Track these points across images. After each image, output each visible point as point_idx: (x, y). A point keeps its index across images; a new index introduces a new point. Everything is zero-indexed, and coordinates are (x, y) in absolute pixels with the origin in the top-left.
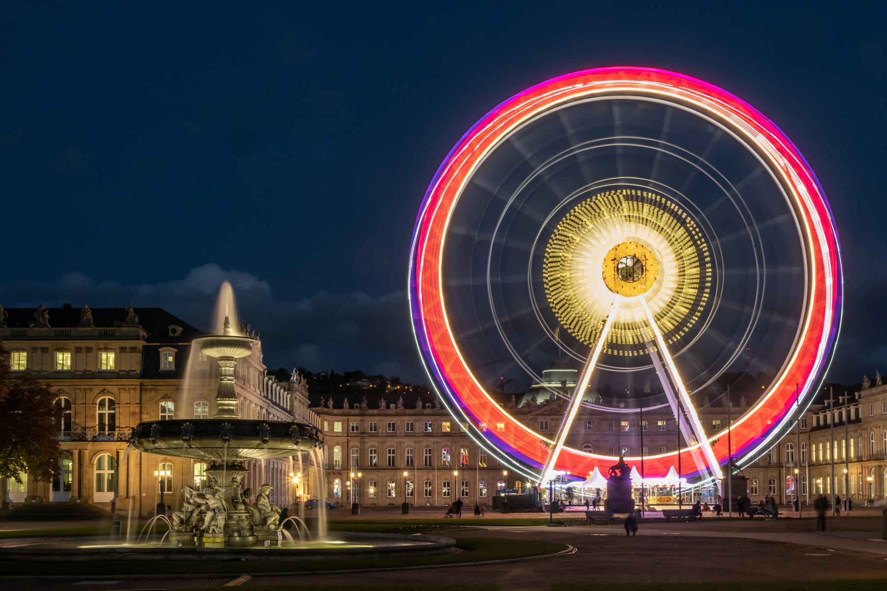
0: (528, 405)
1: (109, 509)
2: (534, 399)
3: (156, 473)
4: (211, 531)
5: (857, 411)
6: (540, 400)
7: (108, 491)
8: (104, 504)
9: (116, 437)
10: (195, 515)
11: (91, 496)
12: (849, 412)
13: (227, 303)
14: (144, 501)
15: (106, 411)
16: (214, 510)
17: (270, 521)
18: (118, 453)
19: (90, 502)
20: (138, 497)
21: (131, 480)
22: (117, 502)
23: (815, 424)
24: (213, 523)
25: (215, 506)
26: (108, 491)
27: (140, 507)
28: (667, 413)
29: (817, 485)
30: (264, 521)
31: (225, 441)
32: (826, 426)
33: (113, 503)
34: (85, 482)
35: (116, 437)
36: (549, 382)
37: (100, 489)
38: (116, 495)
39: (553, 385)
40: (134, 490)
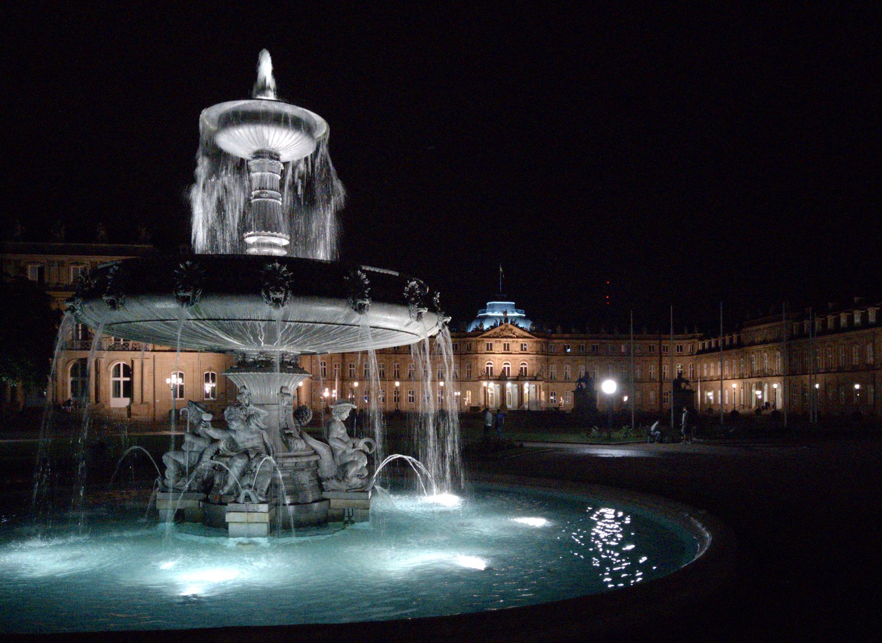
0: (477, 329)
1: (125, 413)
2: (481, 325)
3: (168, 381)
4: (241, 499)
5: (739, 338)
6: (486, 326)
7: (124, 396)
8: (120, 409)
9: (130, 347)
10: (206, 457)
11: (108, 401)
12: (724, 341)
13: (266, 67)
14: (157, 408)
15: (122, 379)
16: (246, 453)
17: (352, 471)
18: (132, 362)
19: (107, 407)
20: (152, 402)
21: (145, 387)
22: (133, 408)
23: (700, 348)
24: (247, 481)
25: (249, 445)
26: (124, 396)
27: (154, 411)
28: (379, 366)
29: (708, 397)
30: (343, 469)
31: (277, 302)
32: (717, 349)
33: (129, 408)
34: (102, 388)
35: (130, 347)
36: (493, 312)
37: (117, 394)
38: (132, 401)
39: (496, 314)
40: (148, 397)
